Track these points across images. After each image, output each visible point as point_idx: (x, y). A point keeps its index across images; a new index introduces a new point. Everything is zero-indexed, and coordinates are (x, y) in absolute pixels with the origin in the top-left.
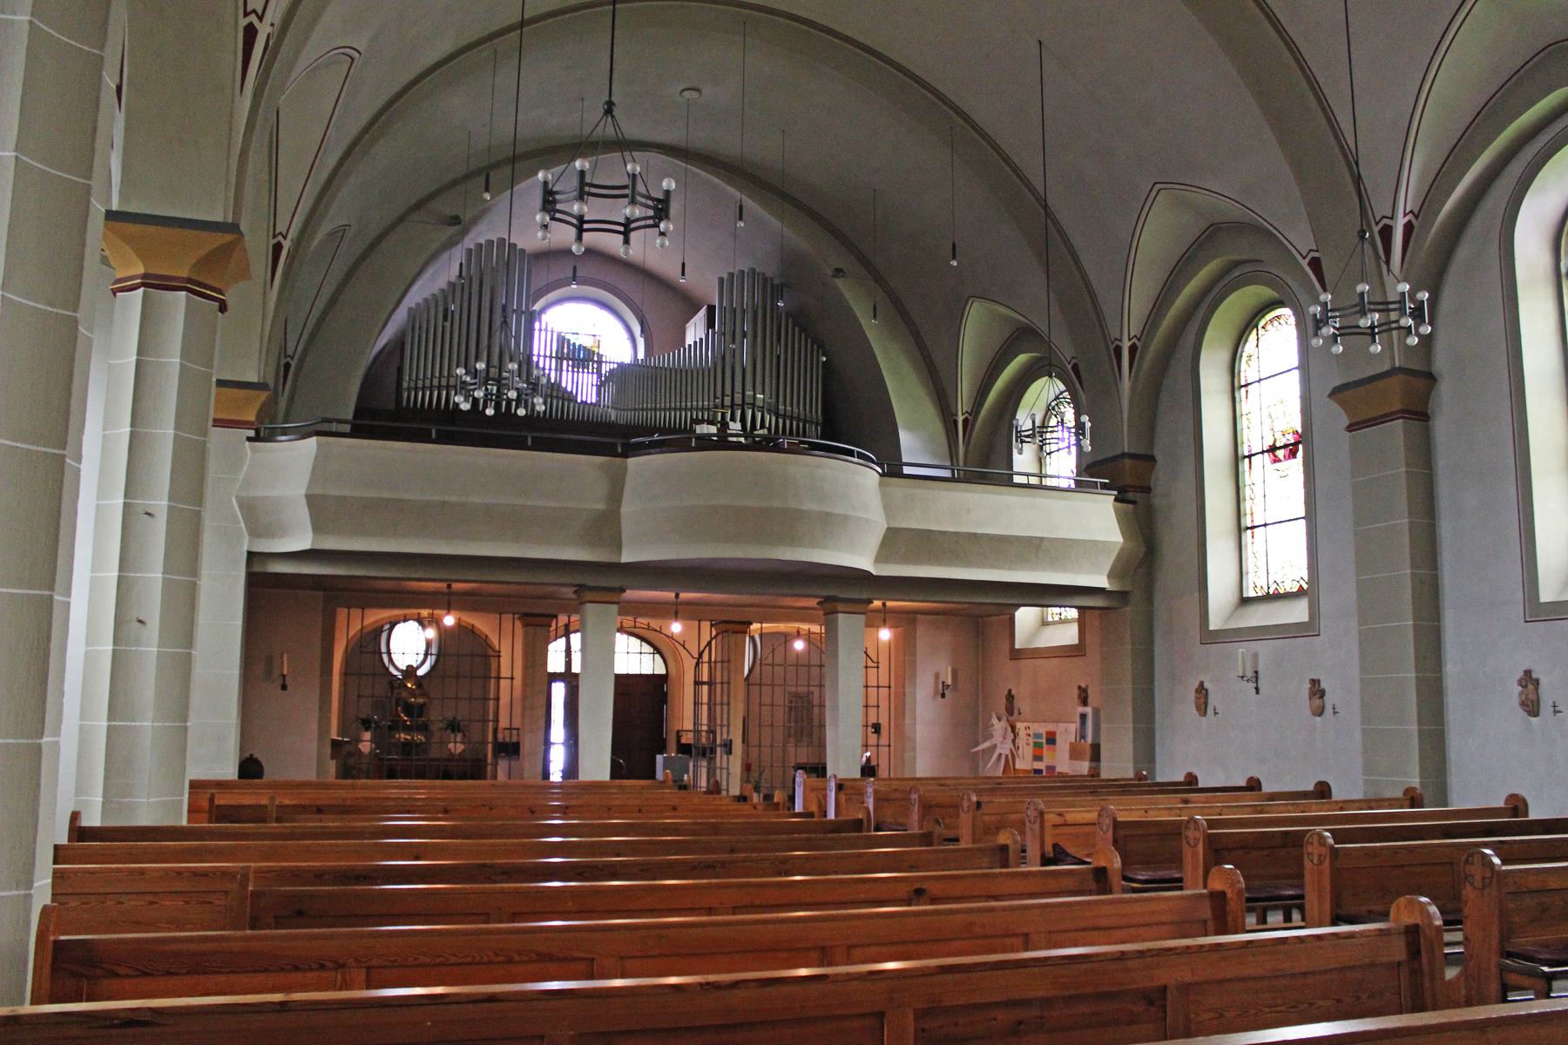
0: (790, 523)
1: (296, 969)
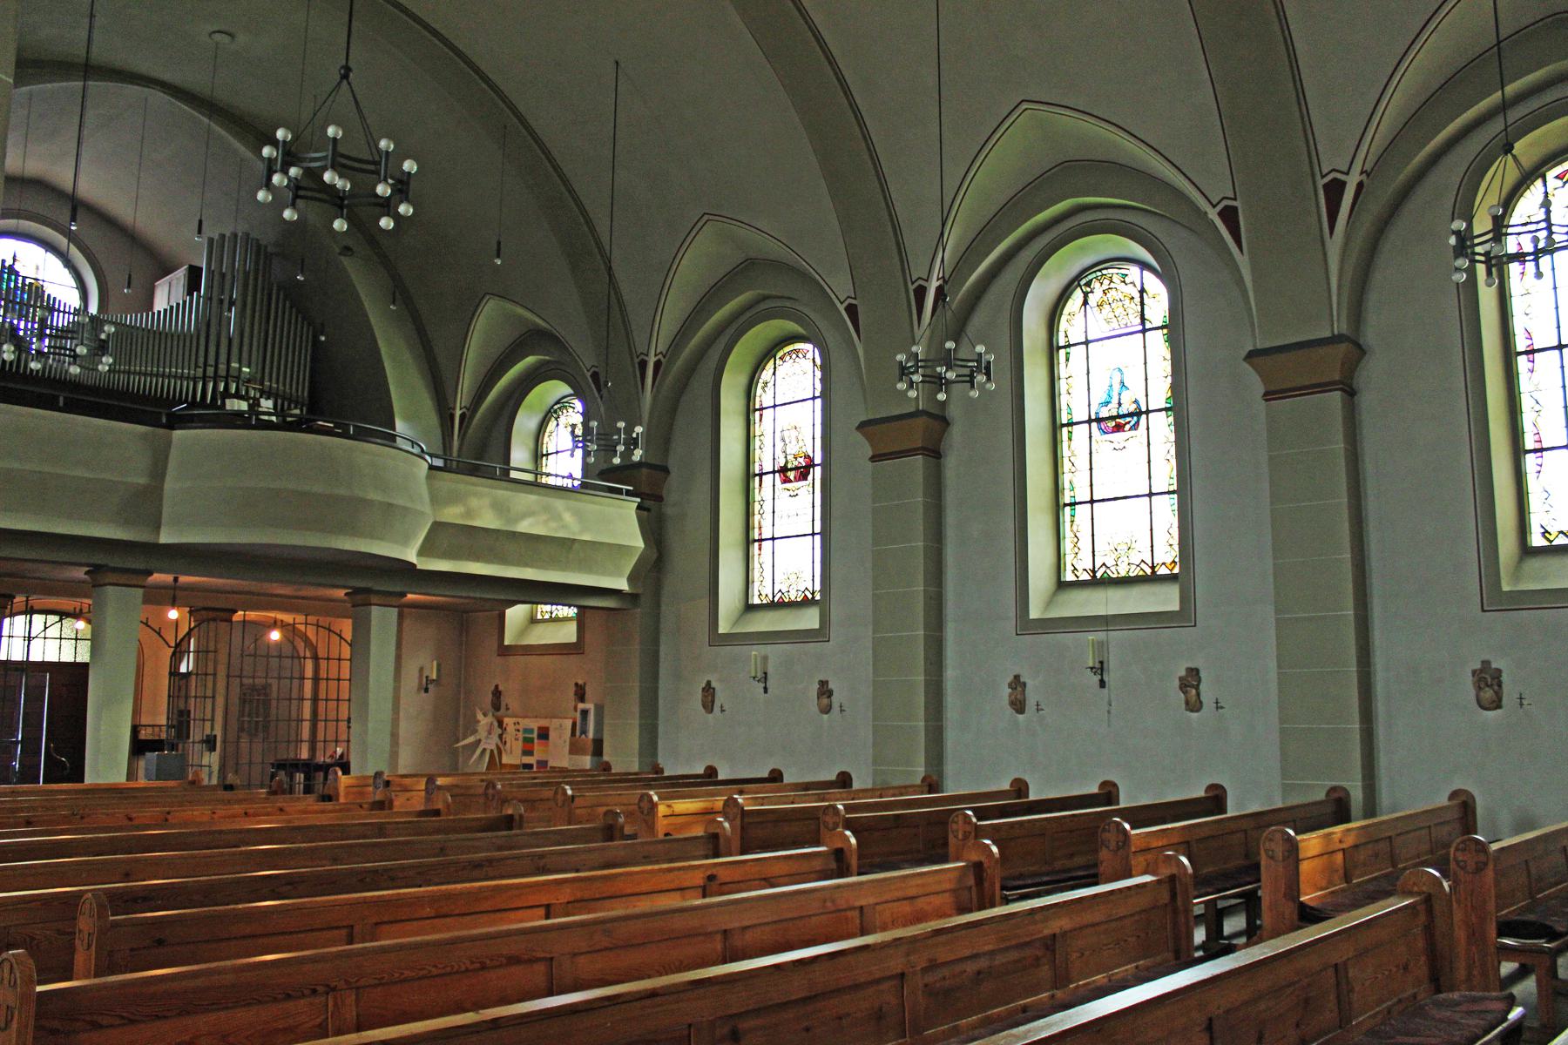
0: (351, 513)
1: (289, 997)
